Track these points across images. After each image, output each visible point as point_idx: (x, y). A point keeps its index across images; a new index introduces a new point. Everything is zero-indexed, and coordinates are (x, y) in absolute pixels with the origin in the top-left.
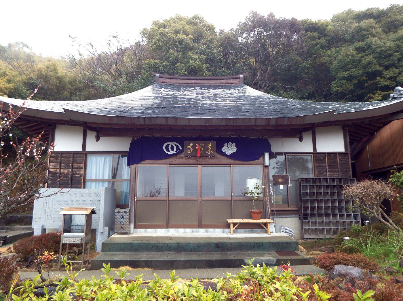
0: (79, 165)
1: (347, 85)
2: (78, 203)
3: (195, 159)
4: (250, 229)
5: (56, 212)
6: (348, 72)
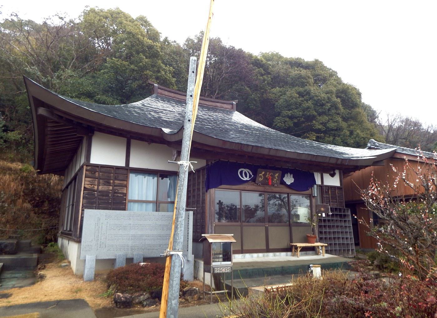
0: (121, 182)
1: (289, 123)
2: (137, 228)
3: (263, 186)
4: (305, 252)
5: (111, 239)
6: (291, 112)
